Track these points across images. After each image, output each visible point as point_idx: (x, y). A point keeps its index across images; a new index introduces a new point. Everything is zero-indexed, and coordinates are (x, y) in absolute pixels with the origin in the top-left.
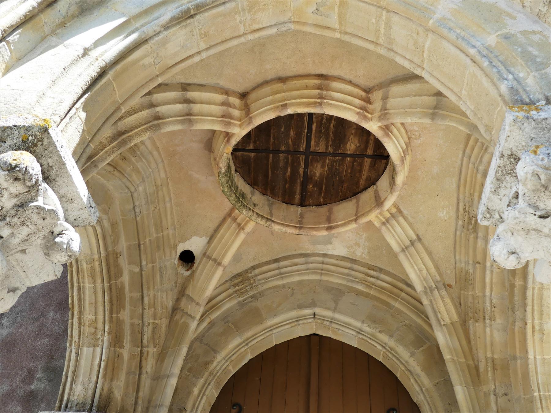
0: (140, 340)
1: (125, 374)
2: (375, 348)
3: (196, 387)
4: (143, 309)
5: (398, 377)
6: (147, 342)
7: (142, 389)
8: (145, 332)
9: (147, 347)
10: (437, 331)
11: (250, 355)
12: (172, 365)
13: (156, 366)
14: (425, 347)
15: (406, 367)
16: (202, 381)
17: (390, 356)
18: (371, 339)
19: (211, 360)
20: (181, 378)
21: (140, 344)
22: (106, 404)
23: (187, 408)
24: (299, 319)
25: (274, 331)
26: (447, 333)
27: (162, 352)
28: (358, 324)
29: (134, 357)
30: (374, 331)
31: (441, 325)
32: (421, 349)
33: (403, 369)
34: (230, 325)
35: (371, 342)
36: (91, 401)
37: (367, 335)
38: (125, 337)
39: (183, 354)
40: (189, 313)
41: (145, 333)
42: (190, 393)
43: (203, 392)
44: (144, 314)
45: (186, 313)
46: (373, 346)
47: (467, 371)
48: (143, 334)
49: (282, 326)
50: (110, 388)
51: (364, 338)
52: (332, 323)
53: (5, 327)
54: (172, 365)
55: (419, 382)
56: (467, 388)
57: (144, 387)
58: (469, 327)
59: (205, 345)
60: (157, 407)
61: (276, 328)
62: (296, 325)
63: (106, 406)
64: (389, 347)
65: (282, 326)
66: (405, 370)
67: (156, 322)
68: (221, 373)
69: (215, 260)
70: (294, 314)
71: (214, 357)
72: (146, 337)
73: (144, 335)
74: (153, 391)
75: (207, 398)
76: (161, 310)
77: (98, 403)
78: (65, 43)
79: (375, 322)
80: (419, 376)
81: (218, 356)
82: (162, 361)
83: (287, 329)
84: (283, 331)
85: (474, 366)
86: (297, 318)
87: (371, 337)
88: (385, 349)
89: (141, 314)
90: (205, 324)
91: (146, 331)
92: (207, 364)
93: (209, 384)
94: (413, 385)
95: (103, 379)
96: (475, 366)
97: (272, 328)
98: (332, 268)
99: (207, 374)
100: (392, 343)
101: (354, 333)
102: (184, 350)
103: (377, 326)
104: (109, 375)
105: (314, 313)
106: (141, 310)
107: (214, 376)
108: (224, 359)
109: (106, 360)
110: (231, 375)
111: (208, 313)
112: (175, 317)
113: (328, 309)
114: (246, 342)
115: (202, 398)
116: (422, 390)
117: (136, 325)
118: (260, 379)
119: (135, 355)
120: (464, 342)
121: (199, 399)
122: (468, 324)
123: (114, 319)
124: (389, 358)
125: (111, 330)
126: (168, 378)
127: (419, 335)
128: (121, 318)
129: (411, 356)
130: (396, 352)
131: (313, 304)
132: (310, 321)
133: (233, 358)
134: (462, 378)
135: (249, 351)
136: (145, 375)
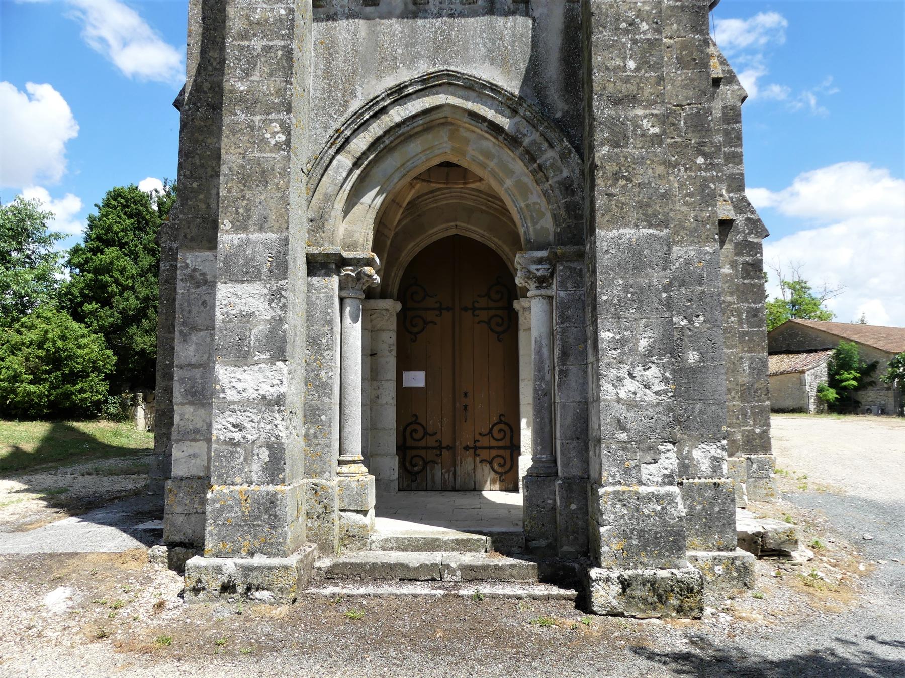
28: (482, 231)
69: (398, 204)
70: (444, 226)
78: (361, 201)
98: (467, 196)
100: (500, 243)
113: (463, 222)
131: (455, 220)
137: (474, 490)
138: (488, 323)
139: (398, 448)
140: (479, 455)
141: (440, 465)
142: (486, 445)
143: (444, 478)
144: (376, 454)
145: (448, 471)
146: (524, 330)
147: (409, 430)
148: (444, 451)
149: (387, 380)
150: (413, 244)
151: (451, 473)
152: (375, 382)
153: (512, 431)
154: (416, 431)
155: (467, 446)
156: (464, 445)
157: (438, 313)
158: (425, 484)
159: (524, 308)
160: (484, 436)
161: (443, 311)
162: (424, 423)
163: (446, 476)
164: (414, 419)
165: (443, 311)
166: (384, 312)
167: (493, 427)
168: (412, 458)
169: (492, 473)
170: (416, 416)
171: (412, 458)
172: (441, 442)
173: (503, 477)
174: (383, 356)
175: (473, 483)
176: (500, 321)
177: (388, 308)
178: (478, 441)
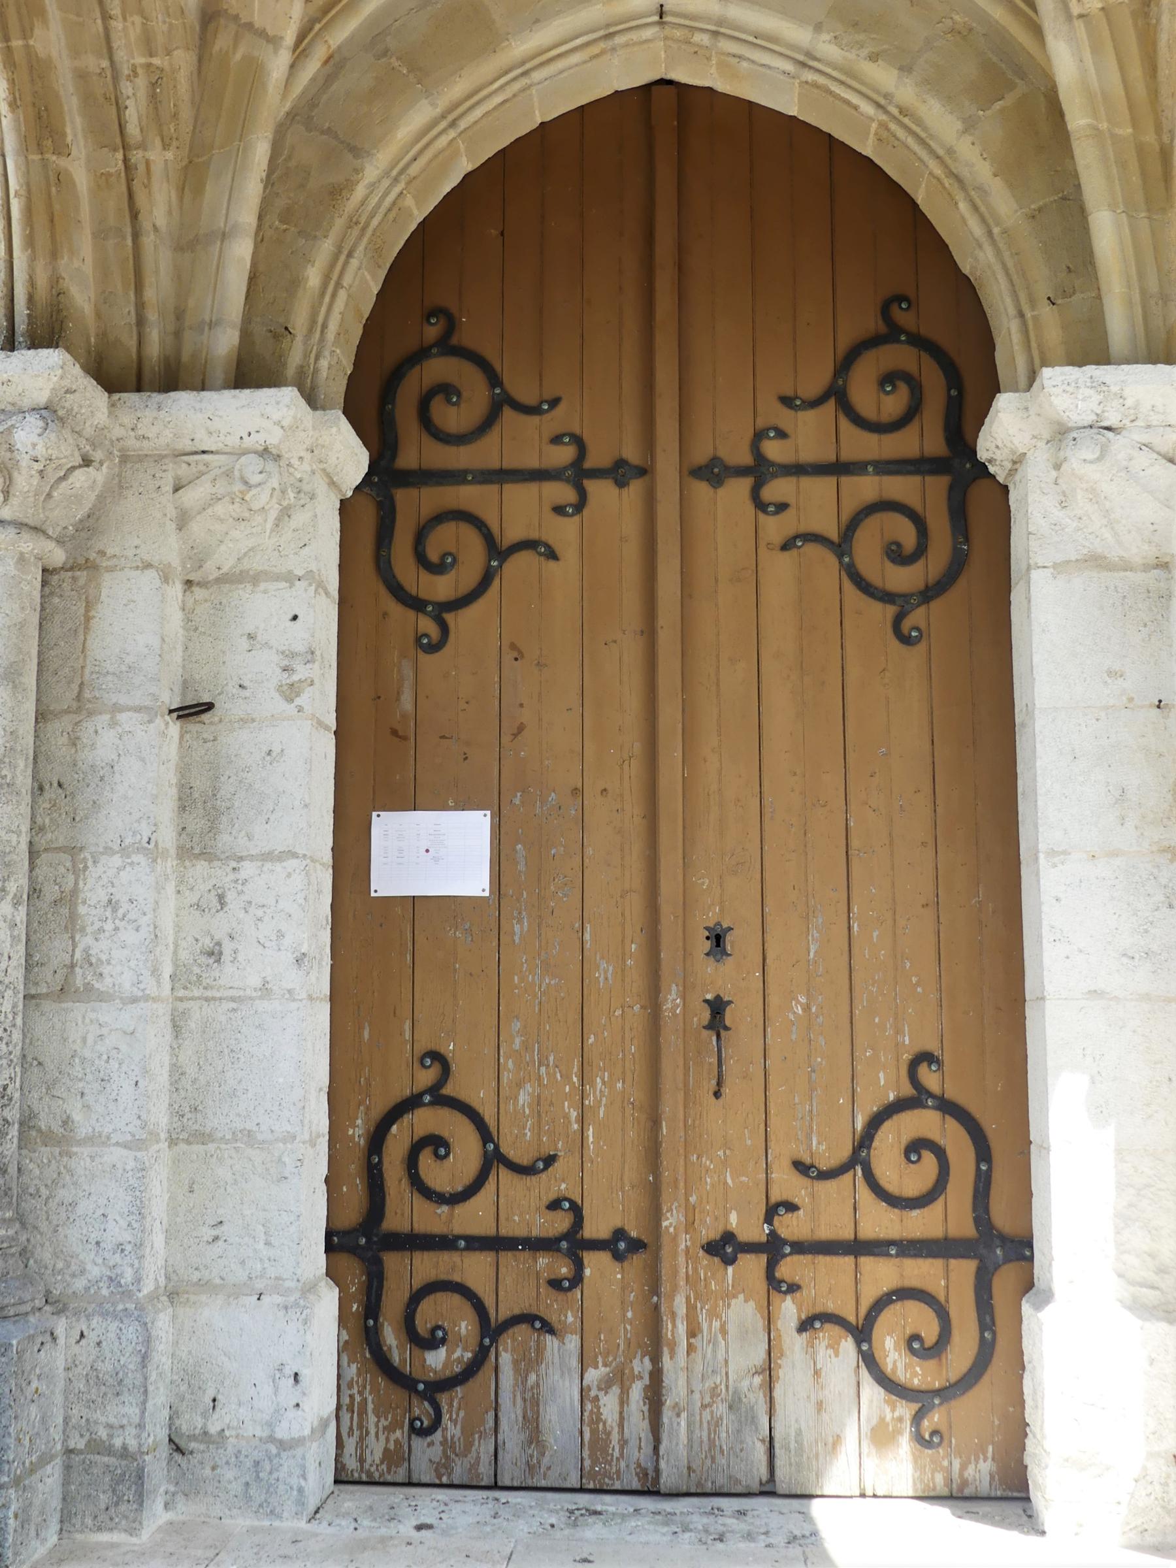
0: (116, 127)
1: (90, 237)
2: (853, 112)
3: (313, 266)
4: (106, 17)
5: (919, 202)
6: (138, 130)
7: (149, 279)
8: (128, 98)
9: (143, 146)
10: (1055, 37)
11: (464, 159)
12: (229, 199)
13: (181, 208)
14: (1010, 100)
15: (946, 166)
16: (326, 247)
17: (901, 133)
18: (842, 83)
19: (347, 180)
20: (262, 240)
21: (118, 140)
22: (53, 328)
23: (294, 329)
24: (612, 30)
25: (537, 76)
26: (1087, 43)
27: (190, 162)
28: (798, 34)
29: (107, 180)
30: (851, 56)
31: (1069, 17)
32: (998, 105)
33: (938, 171)
34: (395, 63)
35: (843, 95)
36: (7, 320)
37: (829, 70)
38: (67, 118)
39: (259, 164)
40: (257, 26)
41: (128, 102)
42: (295, 283)
43: (335, 276)
44: (114, 36)
45: (249, 26)
46: (845, 107)
47: (1134, 166)
48: (122, 106)
49: (560, 56)
50: (55, 280)
51: (822, 80)
52: (720, 38)
53: (163, 1136)
54: (229, 199)
55: (983, 209)
56: (1130, 217)
57: (157, 272)
58: (1158, 20)
59: (323, 132)
60: (206, 328)
61: (542, 64)
62: (603, 53)
63: (53, 333)
64: (898, 106)
65: (560, 56)
66: (943, 176)
67: (156, 61)
68: (382, 220)
71: (357, 171)
72: (132, 115)
73: (126, 108)
74: (183, 282)
75: (349, 296)
76: (164, 22)
77: (29, 324)
79: (857, 24)
80: (985, 192)
81: (367, 165)
82: (199, 191)
83: (577, 65)
84: (565, 74)
85: (1157, 148)
86: (608, 26)
87: (843, 78)
88: (886, 112)
89: (102, 35)
90: (312, 67)
91: (130, 94)
92: (337, 192)
93: (350, 255)
94: (964, 220)
95: (27, 250)
96: (1161, 149)
97: (528, 66)
99: (339, 223)
100: (906, 92)
101: (789, 67)
102: (261, 151)
103: (861, 37)
104: (42, 237)
105: (662, 6)
106: (99, 21)
107: (364, 229)
108: (387, 173)
109: (23, 192)
110: (413, 226)
111: (317, 27)
112: (214, 43)
114: (450, 118)
115: (334, 296)
116: (990, 233)
117: (94, 78)
118: (502, 234)
119: (109, 175)
120: (1136, 72)
121: (327, 299)
122: (1155, 9)
123: (19, 56)
124: (896, 143)
125: (17, 96)
126: (222, 241)
127: (995, 59)
128: (42, 53)
129: (965, 131)
130: (919, 122)
132: (648, 33)
133: (414, 170)
134: (1118, 188)
135: (461, 145)
136: (152, 237)
137: (768, 1490)
138: (842, 546)
139: (335, 1242)
140: (793, 1288)
141: (572, 1342)
142: (836, 1227)
143: (597, 1418)
144: (204, 1286)
145: (620, 1378)
146: (1060, 568)
147: (399, 1137)
148: (596, 1264)
149: (268, 857)
150: (419, 115)
151: (636, 1392)
152: (201, 866)
153: (983, 1151)
154: (437, 1144)
155: (728, 1237)
156: (709, 1231)
157: (564, 493)
158: (485, 1449)
159: (1061, 434)
160: (826, 1175)
161: (594, 487)
162: (480, 1097)
163: (609, 1405)
164: (427, 1077)
165: (591, 486)
166: (251, 466)
167: (876, 1122)
168: (416, 1298)
169: (872, 1392)
170: (437, 1057)
171: (416, 1298)
172: (577, 1210)
173: (935, 1419)
174: (245, 721)
175: (760, 1451)
176: (907, 535)
177: (273, 437)
178: (791, 1207)
